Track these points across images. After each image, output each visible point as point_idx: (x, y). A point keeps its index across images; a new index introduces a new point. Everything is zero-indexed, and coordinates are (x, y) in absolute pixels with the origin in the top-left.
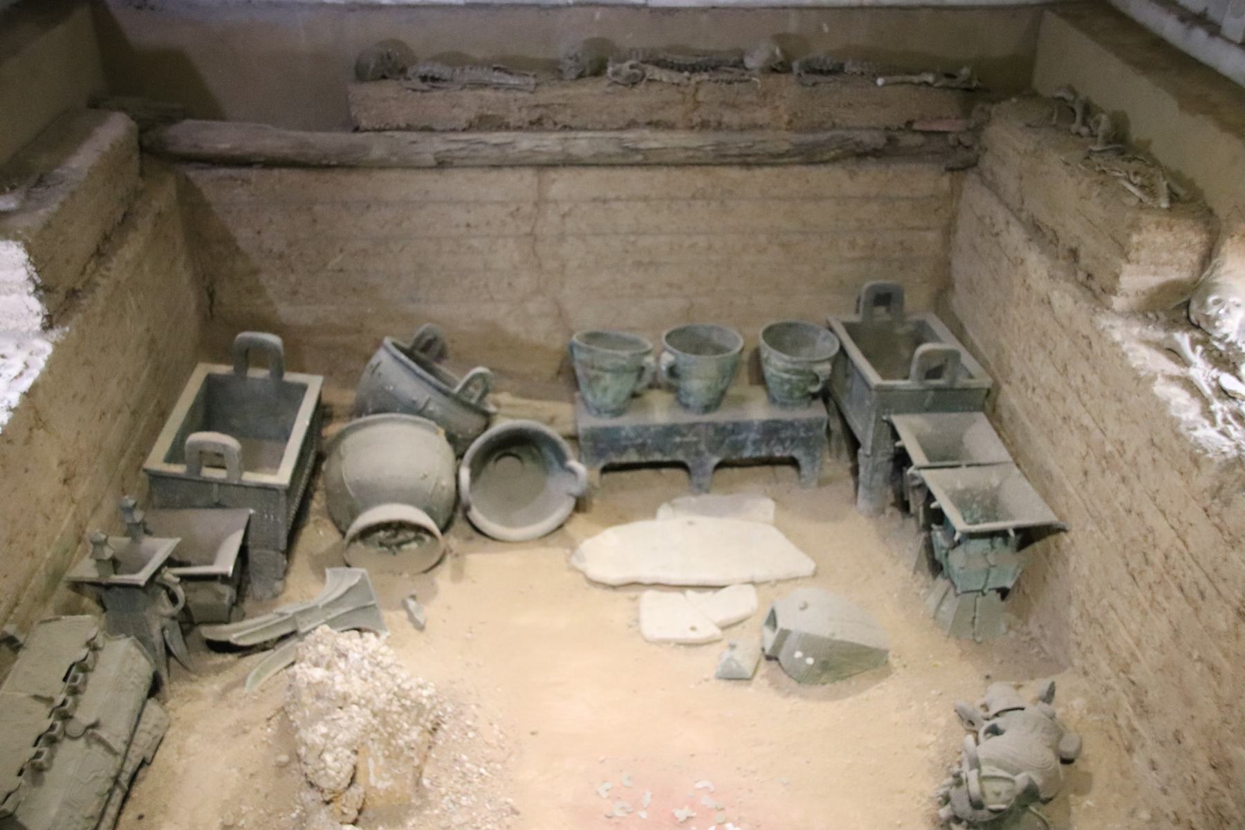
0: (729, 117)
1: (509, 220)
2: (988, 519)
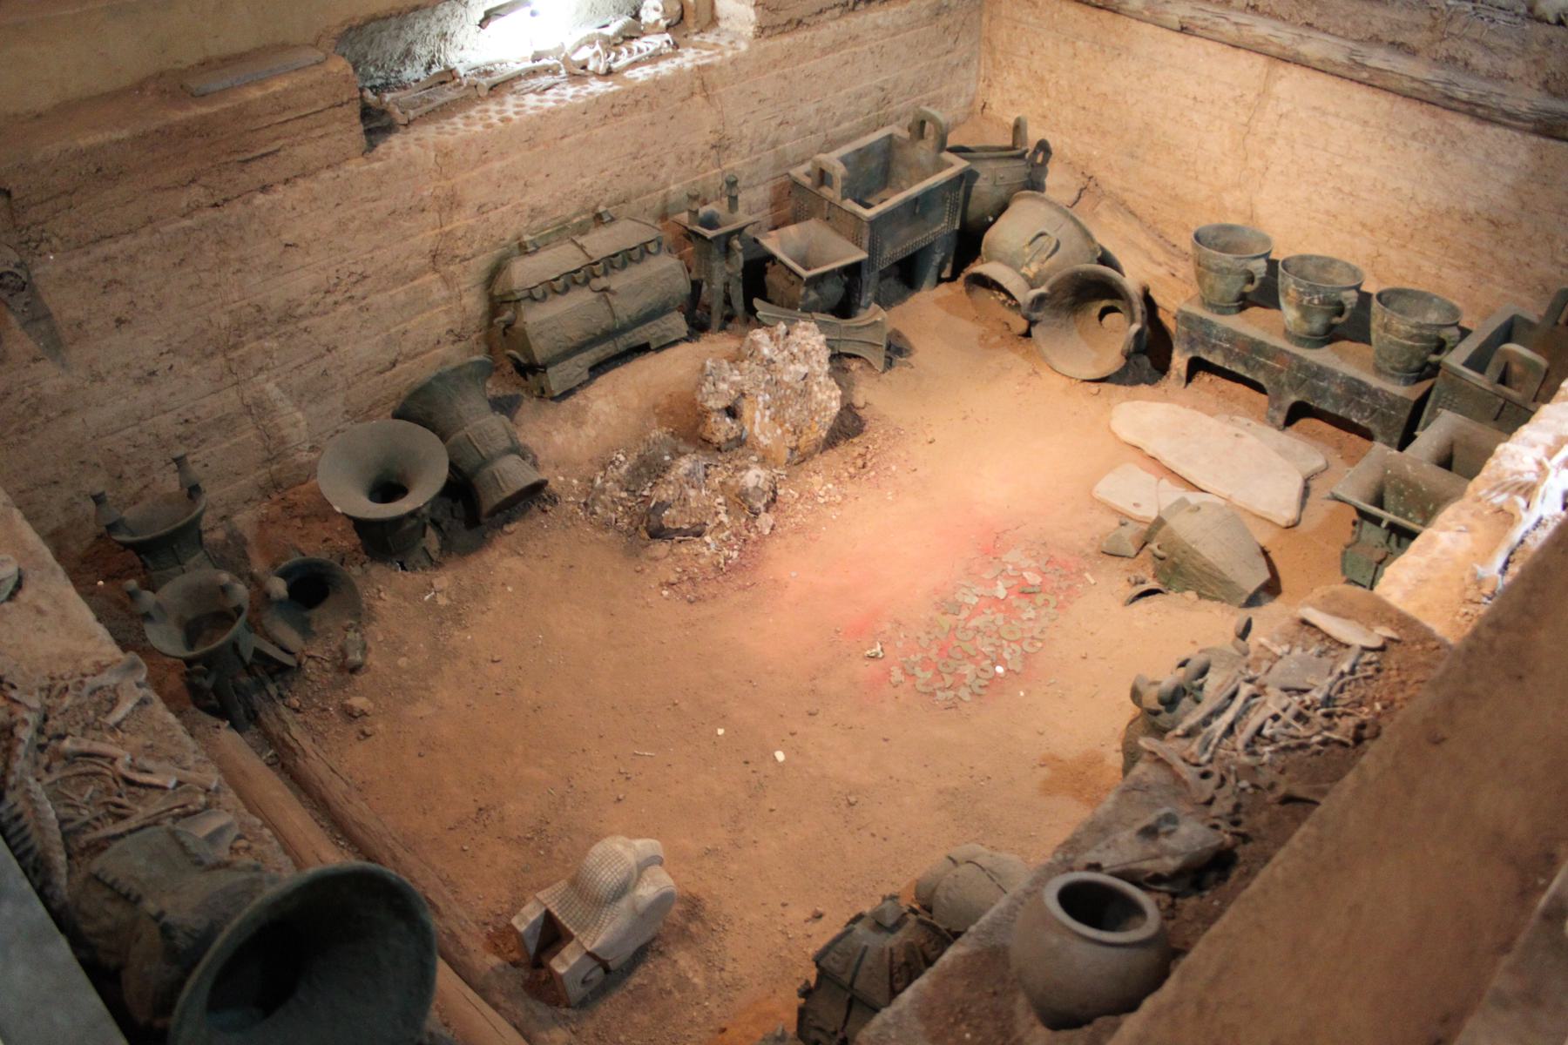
0: (1480, 60)
1: (1231, 104)
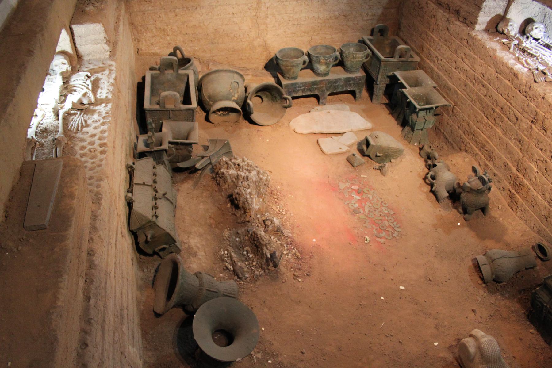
1: (248, 10)
2: (427, 105)
